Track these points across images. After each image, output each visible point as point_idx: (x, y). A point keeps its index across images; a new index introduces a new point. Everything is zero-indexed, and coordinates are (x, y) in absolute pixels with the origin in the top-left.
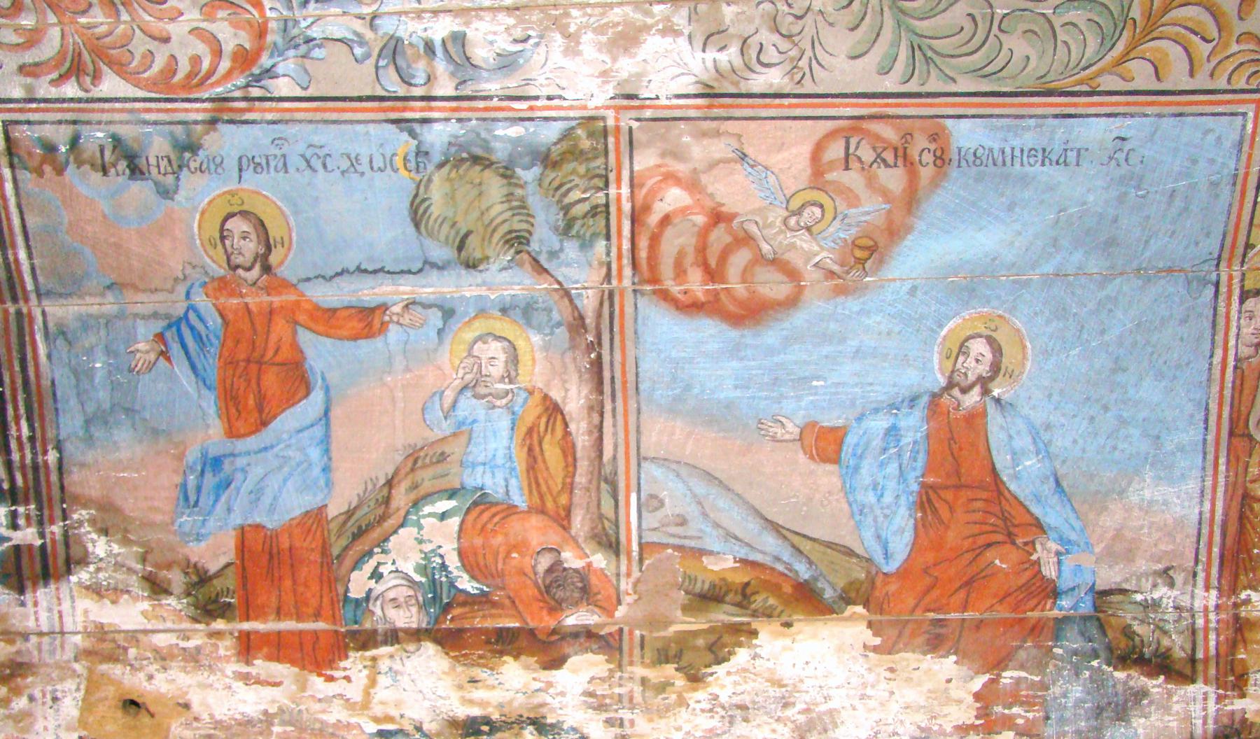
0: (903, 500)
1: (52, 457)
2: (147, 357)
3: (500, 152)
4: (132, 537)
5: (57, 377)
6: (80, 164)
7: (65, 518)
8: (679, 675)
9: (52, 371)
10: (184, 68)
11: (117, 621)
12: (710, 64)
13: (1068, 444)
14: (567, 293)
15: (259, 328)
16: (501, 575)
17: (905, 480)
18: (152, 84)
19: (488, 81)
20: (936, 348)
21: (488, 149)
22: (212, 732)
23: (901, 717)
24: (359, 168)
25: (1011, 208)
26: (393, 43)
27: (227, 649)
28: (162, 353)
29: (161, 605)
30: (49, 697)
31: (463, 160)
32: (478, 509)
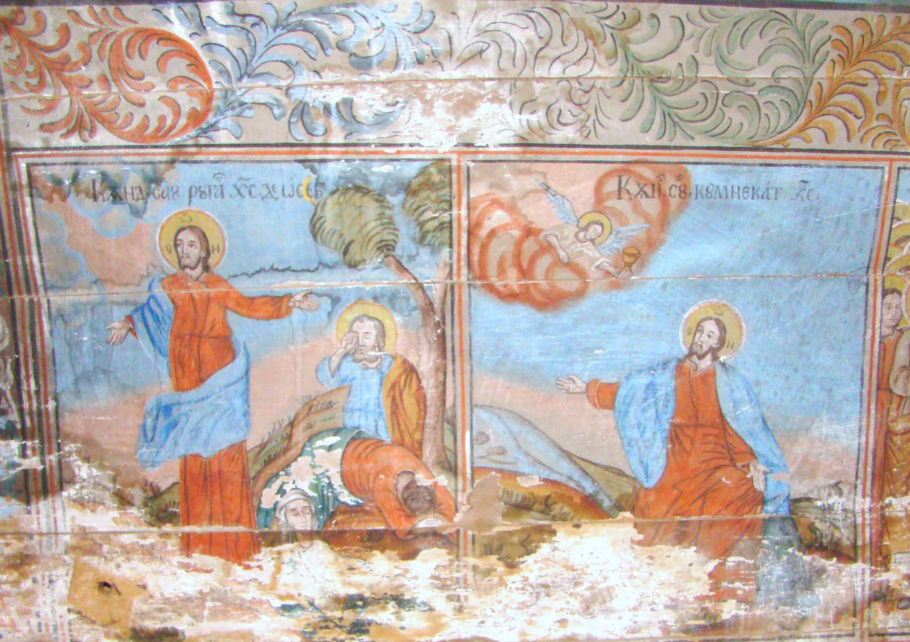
0: (658, 436)
1: (51, 405)
2: (120, 332)
3: (376, 183)
4: (107, 464)
5: (57, 347)
6: (78, 193)
7: (59, 450)
8: (500, 563)
9: (53, 343)
10: (153, 124)
11: (95, 525)
12: (524, 123)
13: (771, 395)
14: (421, 287)
15: (200, 311)
16: (372, 491)
17: (660, 421)
18: (131, 136)
19: (368, 132)
20: (681, 327)
21: (367, 181)
22: (163, 606)
23: (658, 591)
24: (275, 195)
25: (731, 228)
26: (301, 106)
27: (173, 545)
28: (131, 330)
29: (126, 513)
30: (47, 580)
31: (348, 189)
32: (356, 443)
